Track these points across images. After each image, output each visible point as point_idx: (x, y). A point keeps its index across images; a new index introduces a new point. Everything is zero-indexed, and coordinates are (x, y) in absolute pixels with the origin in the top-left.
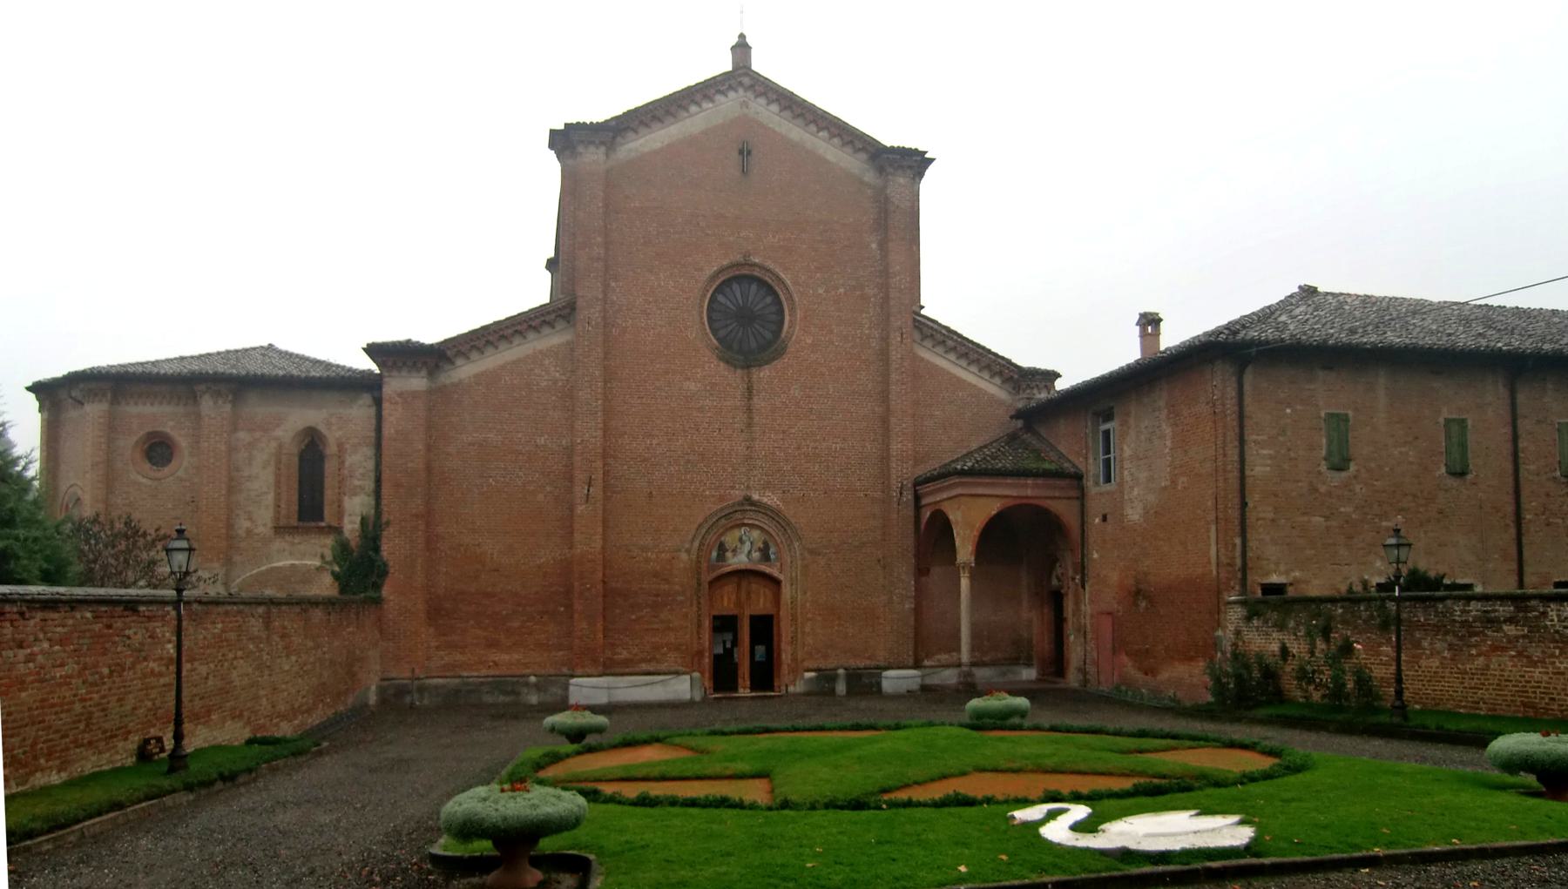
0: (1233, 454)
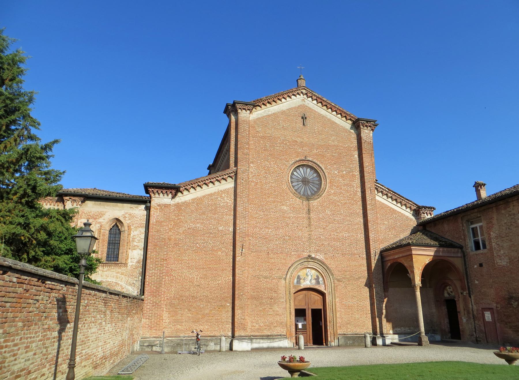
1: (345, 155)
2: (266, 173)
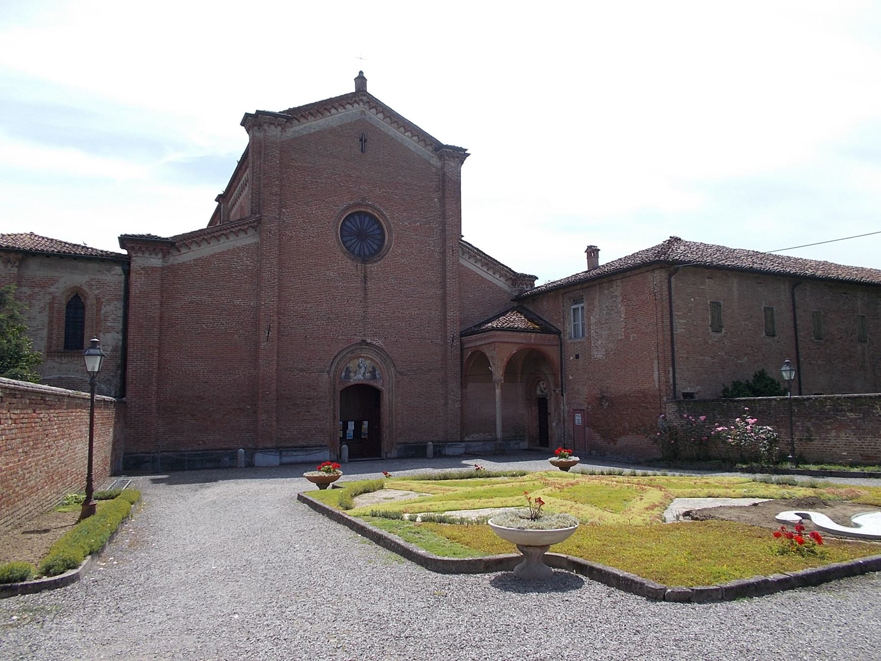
0: (667, 322)
1: (420, 199)
2: (304, 222)
